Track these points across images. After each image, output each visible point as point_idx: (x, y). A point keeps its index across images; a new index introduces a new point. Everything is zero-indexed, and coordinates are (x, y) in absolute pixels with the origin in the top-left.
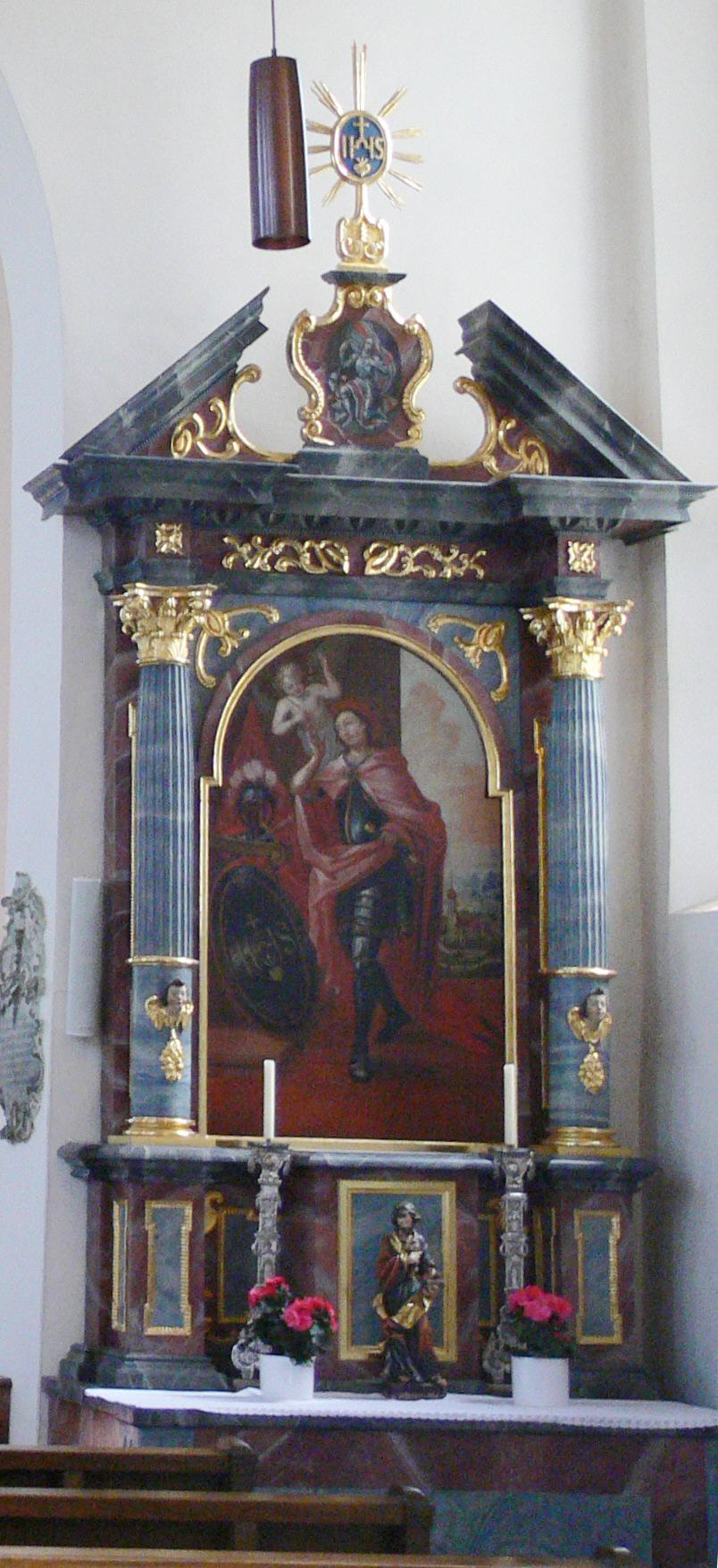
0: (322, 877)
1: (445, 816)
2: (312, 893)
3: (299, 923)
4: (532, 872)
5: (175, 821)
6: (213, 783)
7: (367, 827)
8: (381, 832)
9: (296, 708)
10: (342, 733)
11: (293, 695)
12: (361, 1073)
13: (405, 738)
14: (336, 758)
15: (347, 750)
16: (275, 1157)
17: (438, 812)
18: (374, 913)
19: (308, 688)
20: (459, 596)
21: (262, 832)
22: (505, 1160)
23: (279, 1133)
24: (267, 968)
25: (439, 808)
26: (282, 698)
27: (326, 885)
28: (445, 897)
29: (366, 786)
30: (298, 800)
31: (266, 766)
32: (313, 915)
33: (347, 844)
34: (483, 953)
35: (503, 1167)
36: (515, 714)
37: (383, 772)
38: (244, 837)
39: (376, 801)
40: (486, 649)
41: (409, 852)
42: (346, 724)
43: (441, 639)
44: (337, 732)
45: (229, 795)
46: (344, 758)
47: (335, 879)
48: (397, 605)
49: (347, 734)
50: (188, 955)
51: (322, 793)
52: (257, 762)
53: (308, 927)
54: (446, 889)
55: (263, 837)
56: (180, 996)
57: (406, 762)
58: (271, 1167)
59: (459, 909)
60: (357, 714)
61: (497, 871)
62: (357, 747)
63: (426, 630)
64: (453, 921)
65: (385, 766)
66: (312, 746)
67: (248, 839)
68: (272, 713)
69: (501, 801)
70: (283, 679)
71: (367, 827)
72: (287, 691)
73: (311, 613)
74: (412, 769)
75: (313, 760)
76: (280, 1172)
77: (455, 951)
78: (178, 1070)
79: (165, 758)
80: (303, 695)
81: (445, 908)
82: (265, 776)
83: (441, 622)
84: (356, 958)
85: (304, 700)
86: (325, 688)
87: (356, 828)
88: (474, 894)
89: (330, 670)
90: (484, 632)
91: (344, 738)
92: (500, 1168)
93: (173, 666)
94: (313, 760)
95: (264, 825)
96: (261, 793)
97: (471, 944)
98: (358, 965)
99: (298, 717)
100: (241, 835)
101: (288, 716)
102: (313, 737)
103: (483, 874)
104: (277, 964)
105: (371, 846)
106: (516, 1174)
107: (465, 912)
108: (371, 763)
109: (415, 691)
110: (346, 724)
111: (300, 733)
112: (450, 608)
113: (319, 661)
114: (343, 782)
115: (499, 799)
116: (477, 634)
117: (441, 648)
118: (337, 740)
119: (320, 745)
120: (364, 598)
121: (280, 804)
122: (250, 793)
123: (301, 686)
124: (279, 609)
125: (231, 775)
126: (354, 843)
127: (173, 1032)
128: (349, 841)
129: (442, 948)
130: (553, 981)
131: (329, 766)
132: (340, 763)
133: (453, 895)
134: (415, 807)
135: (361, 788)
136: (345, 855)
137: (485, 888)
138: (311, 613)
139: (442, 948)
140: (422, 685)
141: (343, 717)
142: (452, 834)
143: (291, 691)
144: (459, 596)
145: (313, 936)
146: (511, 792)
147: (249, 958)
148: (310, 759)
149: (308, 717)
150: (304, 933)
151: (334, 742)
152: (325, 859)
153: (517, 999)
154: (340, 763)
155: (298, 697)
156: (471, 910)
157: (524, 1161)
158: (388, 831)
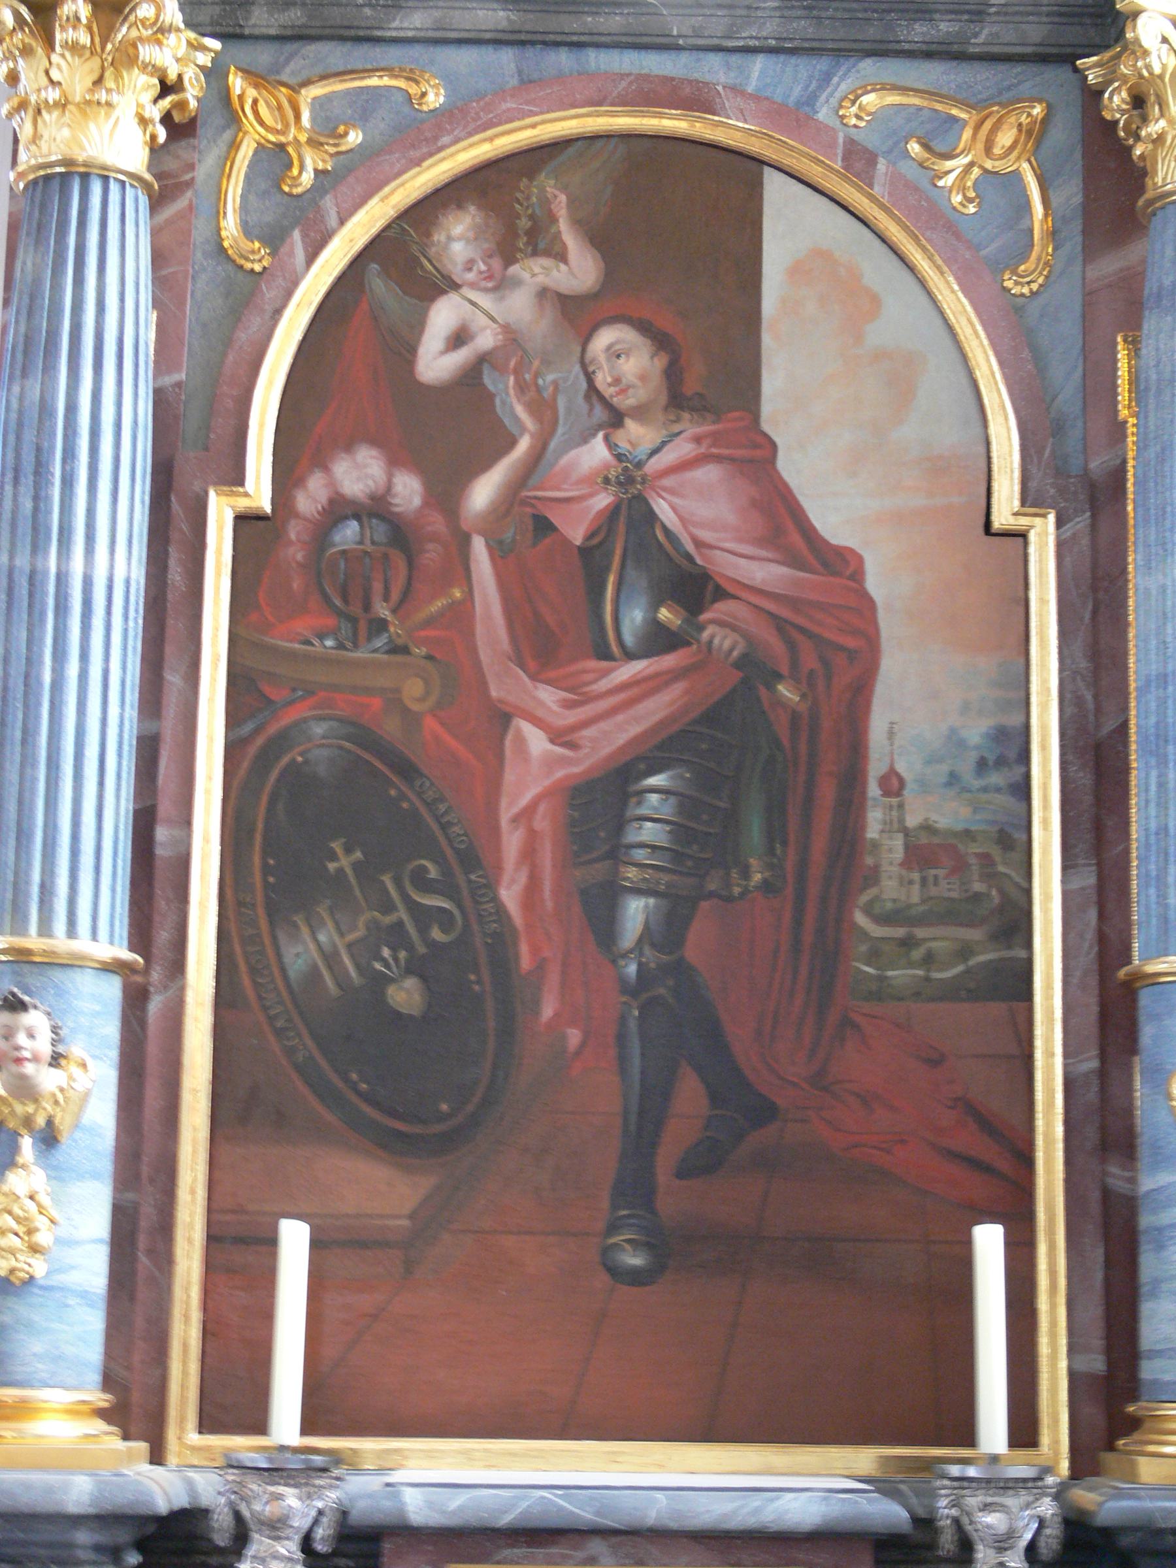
0: (537, 742)
1: (874, 584)
2: (510, 776)
3: (470, 859)
4: (1109, 726)
5: (62, 579)
6: (243, 504)
7: (664, 614)
8: (701, 628)
9: (483, 320)
10: (602, 379)
11: (473, 286)
12: (634, 1260)
13: (772, 384)
14: (585, 438)
15: (616, 419)
16: (291, 1498)
17: (858, 575)
18: (682, 832)
19: (514, 269)
20: (919, 32)
21: (381, 625)
22: (973, 1501)
23: (309, 1426)
24: (379, 982)
25: (860, 560)
26: (443, 292)
27: (551, 763)
28: (873, 790)
29: (662, 508)
30: (479, 545)
31: (394, 462)
32: (512, 842)
33: (606, 656)
34: (975, 935)
35: (965, 1520)
36: (1069, 327)
37: (709, 474)
38: (329, 643)
39: (690, 547)
40: (989, 164)
41: (778, 677)
42: (615, 354)
43: (871, 141)
44: (589, 378)
45: (293, 536)
46: (606, 439)
47: (572, 746)
48: (759, 63)
49: (617, 381)
50: (121, 946)
51: (543, 526)
52: (374, 452)
53: (499, 868)
54: (875, 768)
55: (380, 642)
56: (21, 1039)
57: (773, 446)
58: (276, 1527)
59: (912, 821)
60: (644, 327)
61: (1016, 720)
62: (640, 413)
63: (836, 124)
64: (896, 847)
65: (718, 459)
66: (520, 410)
67: (341, 646)
68: (418, 325)
69: (1026, 544)
70: (446, 247)
71: (664, 614)
72: (458, 274)
73: (526, 82)
74: (790, 466)
75: (524, 445)
76: (307, 1544)
77: (900, 932)
78: (35, 1249)
79: (46, 409)
80: (500, 285)
81: (874, 821)
82: (389, 487)
83: (870, 100)
84: (624, 956)
85: (502, 298)
86: (563, 267)
87: (635, 617)
88: (953, 779)
89: (578, 223)
90: (988, 125)
91: (608, 392)
92: (956, 1521)
93: (105, 179)
94: (524, 445)
95: (382, 610)
96: (380, 531)
97: (949, 914)
98: (632, 969)
99: (486, 340)
100: (321, 637)
101: (458, 339)
102: (521, 388)
103: (976, 732)
104: (409, 971)
105: (669, 661)
106: (1003, 1543)
107: (927, 828)
108: (681, 449)
109: (797, 271)
110: (615, 354)
111: (489, 379)
112: (892, 69)
113: (546, 202)
114: (603, 501)
115: (1022, 536)
116: (967, 134)
117: (871, 159)
118: (587, 397)
119: (543, 409)
120: (667, 46)
121: (431, 555)
122: (348, 533)
123: (496, 263)
124: (450, 81)
125: (300, 482)
126: (630, 656)
127: (27, 1143)
128: (615, 649)
129: (860, 919)
130: (1145, 998)
131: (564, 461)
132: (596, 453)
133: (893, 784)
134: (793, 560)
135: (651, 517)
136: (604, 685)
137: (982, 765)
138: (526, 82)
139: (860, 919)
140: (821, 255)
141: (605, 338)
142: (889, 626)
143: (471, 276)
144: (919, 32)
145: (510, 895)
146: (1052, 518)
147: (331, 958)
148: (512, 443)
149: (512, 337)
150: (490, 887)
151: (580, 400)
152: (548, 696)
153: (1066, 1055)
154: (596, 453)
155: (486, 290)
156: (943, 821)
157: (1028, 1506)
158: (721, 624)
